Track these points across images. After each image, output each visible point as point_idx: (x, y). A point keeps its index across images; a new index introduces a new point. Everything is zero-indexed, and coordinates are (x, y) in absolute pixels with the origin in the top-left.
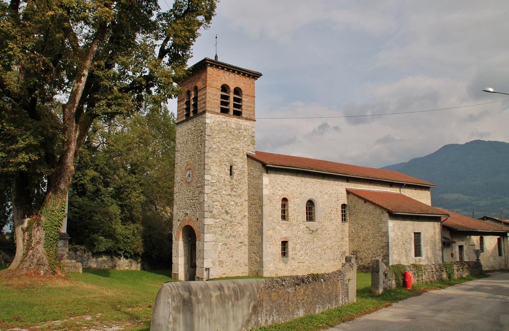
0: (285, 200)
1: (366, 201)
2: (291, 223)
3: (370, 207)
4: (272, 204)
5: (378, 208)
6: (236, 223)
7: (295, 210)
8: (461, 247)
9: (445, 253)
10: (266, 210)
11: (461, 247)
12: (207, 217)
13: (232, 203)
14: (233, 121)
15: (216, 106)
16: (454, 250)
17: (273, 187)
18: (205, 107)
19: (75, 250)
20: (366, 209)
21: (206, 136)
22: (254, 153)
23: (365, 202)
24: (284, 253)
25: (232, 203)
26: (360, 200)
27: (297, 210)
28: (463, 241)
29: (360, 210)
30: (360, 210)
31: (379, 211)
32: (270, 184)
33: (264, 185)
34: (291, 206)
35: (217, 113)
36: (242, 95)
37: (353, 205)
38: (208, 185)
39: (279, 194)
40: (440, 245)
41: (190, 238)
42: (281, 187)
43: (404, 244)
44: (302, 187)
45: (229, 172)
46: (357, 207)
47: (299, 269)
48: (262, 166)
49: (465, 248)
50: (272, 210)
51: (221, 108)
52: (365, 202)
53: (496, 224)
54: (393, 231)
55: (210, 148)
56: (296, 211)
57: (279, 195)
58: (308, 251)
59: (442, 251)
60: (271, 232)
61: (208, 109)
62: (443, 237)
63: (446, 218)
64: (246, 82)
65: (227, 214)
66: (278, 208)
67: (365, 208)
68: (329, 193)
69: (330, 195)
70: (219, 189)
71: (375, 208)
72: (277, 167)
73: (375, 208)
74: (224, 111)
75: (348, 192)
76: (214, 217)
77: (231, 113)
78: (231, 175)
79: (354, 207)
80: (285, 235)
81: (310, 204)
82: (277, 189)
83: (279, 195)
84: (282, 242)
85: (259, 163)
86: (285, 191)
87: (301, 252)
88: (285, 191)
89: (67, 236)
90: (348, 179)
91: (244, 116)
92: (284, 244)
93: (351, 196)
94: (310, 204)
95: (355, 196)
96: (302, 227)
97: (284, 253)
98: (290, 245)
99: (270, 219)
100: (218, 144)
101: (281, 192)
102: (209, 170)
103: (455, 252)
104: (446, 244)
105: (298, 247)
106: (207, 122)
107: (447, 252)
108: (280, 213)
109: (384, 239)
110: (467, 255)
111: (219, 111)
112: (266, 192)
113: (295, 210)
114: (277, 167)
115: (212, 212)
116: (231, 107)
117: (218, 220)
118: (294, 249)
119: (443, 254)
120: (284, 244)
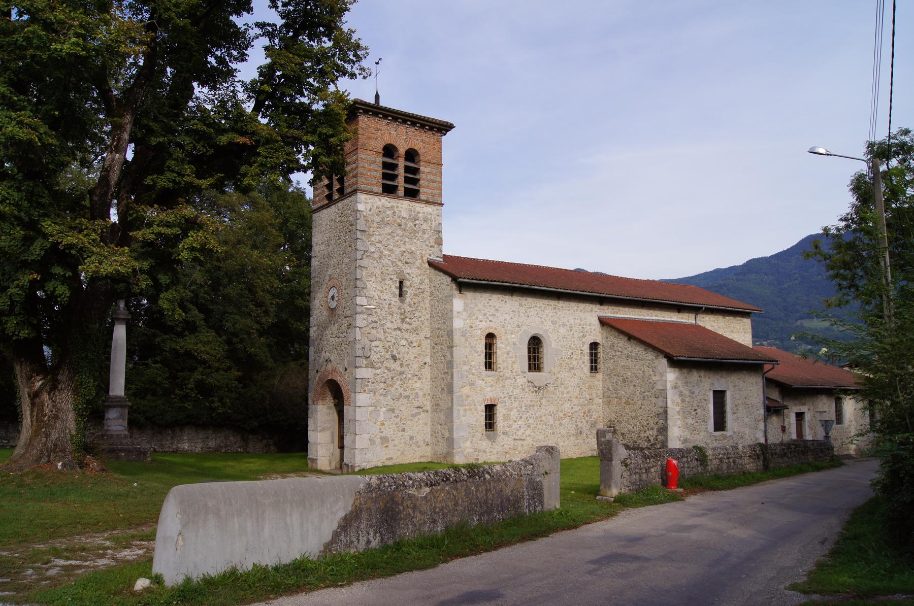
0: (490, 336)
2: (501, 374)
6: (409, 376)
8: (800, 416)
9: (770, 426)
10: (460, 353)
11: (800, 416)
14: (404, 206)
15: (375, 181)
24: (490, 424)
25: (403, 342)
27: (511, 352)
32: (465, 310)
35: (376, 194)
39: (480, 327)
40: (762, 411)
42: (485, 315)
45: (397, 292)
49: (808, 417)
58: (531, 421)
59: (765, 422)
66: (479, 350)
74: (389, 190)
77: (401, 192)
87: (520, 423)
90: (602, 301)
91: (423, 197)
92: (490, 409)
94: (535, 344)
97: (490, 424)
99: (465, 368)
101: (484, 323)
103: (790, 424)
104: (772, 410)
105: (514, 414)
110: (811, 429)
111: (380, 189)
112: (458, 324)
118: (506, 418)
119: (765, 426)
120: (490, 409)
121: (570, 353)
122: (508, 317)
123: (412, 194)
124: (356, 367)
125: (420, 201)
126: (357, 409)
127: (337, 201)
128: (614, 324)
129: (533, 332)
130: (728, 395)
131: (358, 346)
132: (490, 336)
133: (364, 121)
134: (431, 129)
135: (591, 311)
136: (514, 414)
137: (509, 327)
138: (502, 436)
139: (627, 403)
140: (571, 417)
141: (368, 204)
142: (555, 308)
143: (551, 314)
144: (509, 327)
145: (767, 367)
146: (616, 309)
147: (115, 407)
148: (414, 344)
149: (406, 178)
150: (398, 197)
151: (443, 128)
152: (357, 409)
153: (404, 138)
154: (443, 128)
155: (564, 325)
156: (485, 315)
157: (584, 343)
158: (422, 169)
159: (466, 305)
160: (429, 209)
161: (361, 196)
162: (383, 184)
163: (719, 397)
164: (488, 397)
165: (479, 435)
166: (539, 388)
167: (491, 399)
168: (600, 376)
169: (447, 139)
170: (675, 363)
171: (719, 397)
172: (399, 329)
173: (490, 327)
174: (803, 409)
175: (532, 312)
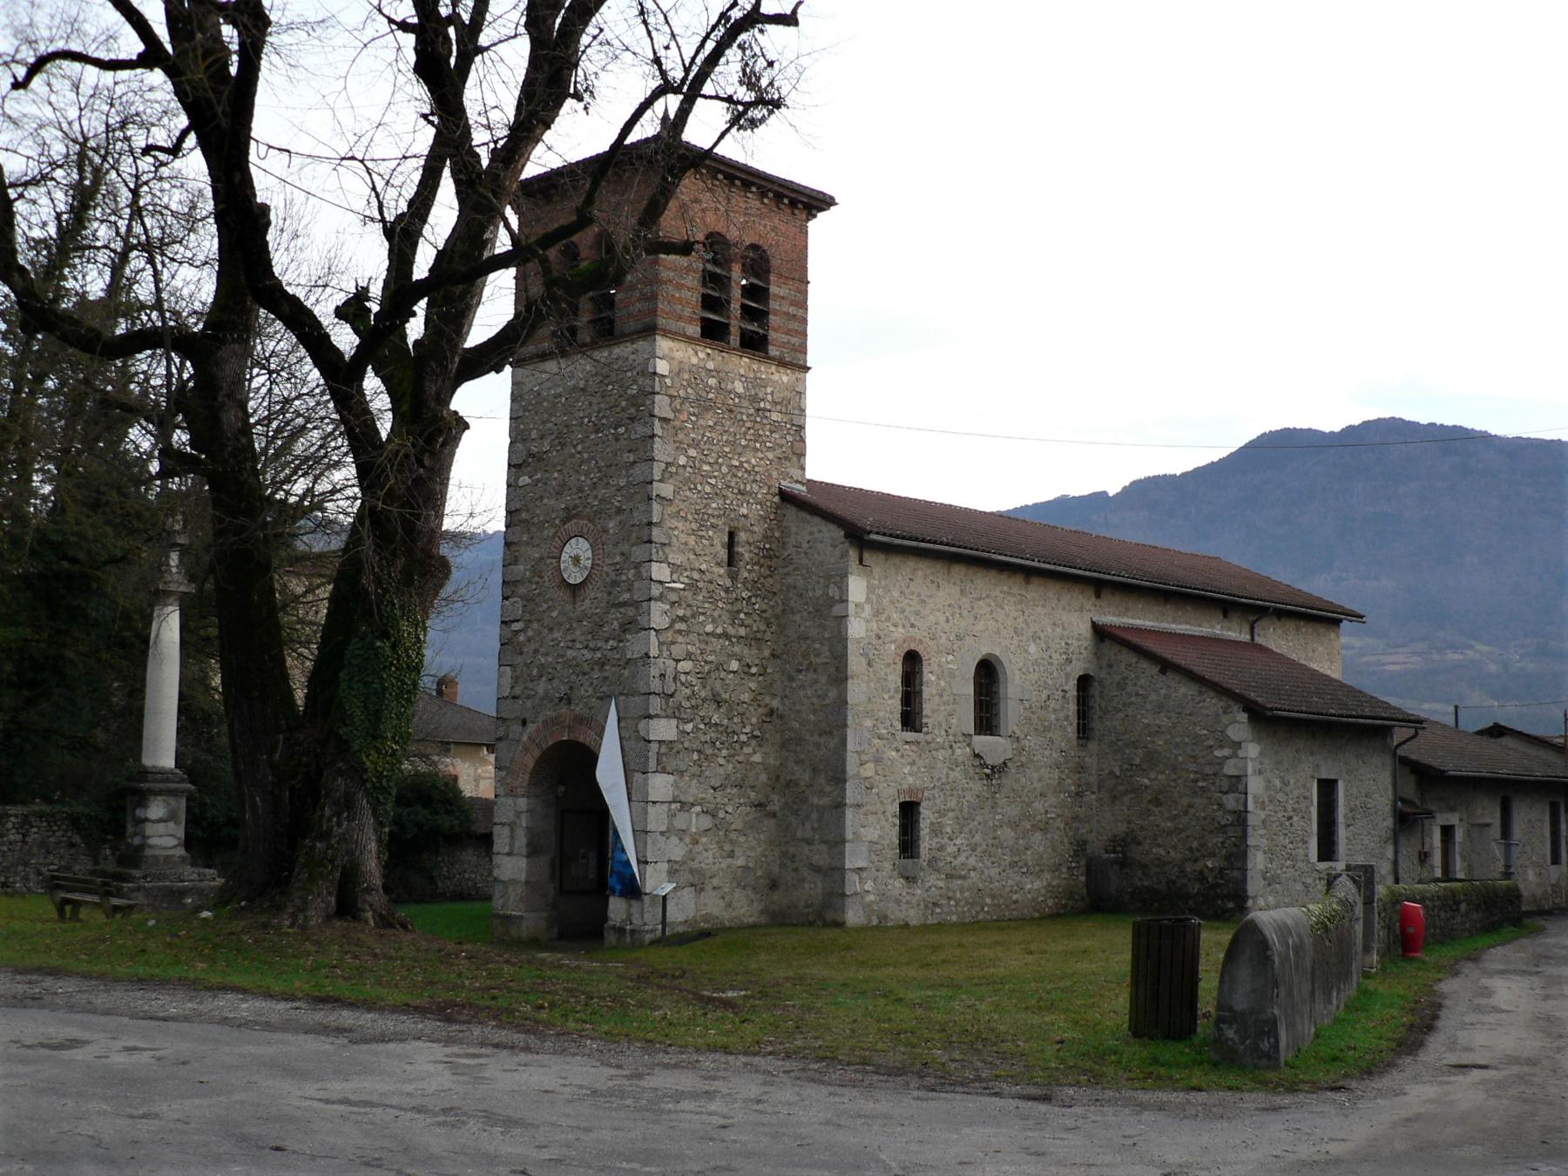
0: (912, 660)
1: (1166, 666)
2: (929, 738)
3: (1183, 690)
4: (875, 673)
5: (1212, 694)
6: (744, 738)
7: (941, 696)
8: (1447, 832)
9: (1403, 851)
10: (856, 692)
11: (1447, 832)
12: (657, 716)
13: (734, 665)
14: (742, 364)
15: (687, 312)
16: (1427, 840)
17: (877, 613)
18: (653, 312)
19: (1280, 763)
20: (1167, 697)
21: (656, 422)
22: (804, 488)
23: (1163, 671)
24: (908, 845)
25: (734, 665)
26: (1145, 665)
27: (949, 693)
28: (1452, 809)
29: (1145, 697)
30: (1145, 697)
31: (1212, 703)
32: (868, 600)
33: (851, 607)
34: (930, 677)
35: (690, 340)
36: (768, 271)
37: (1117, 678)
38: (661, 598)
39: (895, 636)
40: (1390, 822)
41: (562, 789)
42: (903, 611)
43: (1290, 818)
44: (965, 613)
45: (723, 554)
46: (1130, 688)
47: (949, 898)
48: (847, 536)
49: (1459, 835)
50: (871, 692)
51: (704, 320)
52: (1163, 671)
53: (1532, 751)
54: (1260, 772)
55: (668, 464)
56: (945, 698)
57: (894, 642)
58: (978, 838)
59: (1396, 843)
60: (869, 770)
61: (661, 322)
62: (1398, 797)
63: (1412, 731)
64: (782, 227)
65: (719, 704)
66: (892, 686)
67: (1163, 691)
68: (1042, 635)
69: (1046, 642)
70: (693, 616)
71: (1201, 693)
72: (923, 545)
73: (1201, 693)
74: (713, 333)
75: (1101, 633)
76: (676, 714)
77: (735, 339)
78: (730, 564)
79: (1121, 685)
80: (911, 780)
81: (987, 672)
82: (888, 619)
83: (894, 642)
84: (902, 805)
85: (832, 527)
86: (913, 626)
87: (958, 842)
88: (913, 626)
89: (183, 781)
90: (1099, 586)
91: (773, 351)
92: (909, 811)
93: (1110, 650)
94: (987, 672)
95: (1125, 650)
96: (962, 752)
97: (908, 845)
98: (926, 817)
99: (868, 723)
100: (692, 452)
101: (901, 630)
102: (664, 544)
103: (1432, 847)
104: (1406, 821)
105: (949, 824)
106: (659, 370)
107: (1409, 851)
108: (895, 704)
109: (1230, 802)
110: (1463, 857)
111: (694, 330)
112: (856, 628)
113: (941, 696)
114: (923, 545)
115: (672, 696)
116: (736, 324)
117: (689, 727)
118: (936, 830)
119: (1396, 852)
120: (909, 811)
121: (1044, 697)
122: (942, 619)
123: (755, 344)
124: (650, 717)
125: (768, 358)
126: (650, 808)
127: (583, 349)
128: (1135, 640)
129: (984, 650)
130: (1341, 786)
131: (654, 671)
132: (912, 660)
133: (689, 186)
134: (793, 204)
135: (1081, 609)
136: (949, 824)
137: (943, 640)
138: (506, 859)
139: (1157, 802)
140: (1044, 831)
141: (672, 356)
142: (1021, 602)
143: (1014, 614)
144: (943, 640)
145: (1399, 734)
146: (1169, 610)
147: (160, 793)
148: (754, 670)
149: (743, 306)
150: (730, 350)
151: (816, 203)
152: (650, 808)
153: (745, 222)
154: (816, 203)
155: (1035, 638)
156: (903, 611)
157: (1068, 676)
158: (773, 289)
159: (870, 589)
160: (785, 377)
161: (663, 344)
162: (704, 320)
163: (1327, 788)
164: (905, 786)
165: (888, 866)
166: (993, 768)
167: (910, 791)
168: (1093, 746)
169: (819, 227)
170: (1260, 717)
171: (1327, 788)
172: (726, 635)
173: (913, 639)
174: (1453, 819)
175: (982, 607)
